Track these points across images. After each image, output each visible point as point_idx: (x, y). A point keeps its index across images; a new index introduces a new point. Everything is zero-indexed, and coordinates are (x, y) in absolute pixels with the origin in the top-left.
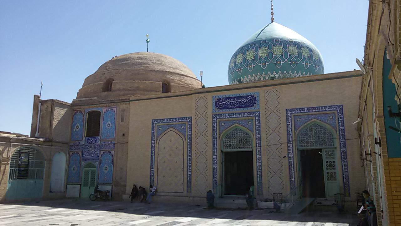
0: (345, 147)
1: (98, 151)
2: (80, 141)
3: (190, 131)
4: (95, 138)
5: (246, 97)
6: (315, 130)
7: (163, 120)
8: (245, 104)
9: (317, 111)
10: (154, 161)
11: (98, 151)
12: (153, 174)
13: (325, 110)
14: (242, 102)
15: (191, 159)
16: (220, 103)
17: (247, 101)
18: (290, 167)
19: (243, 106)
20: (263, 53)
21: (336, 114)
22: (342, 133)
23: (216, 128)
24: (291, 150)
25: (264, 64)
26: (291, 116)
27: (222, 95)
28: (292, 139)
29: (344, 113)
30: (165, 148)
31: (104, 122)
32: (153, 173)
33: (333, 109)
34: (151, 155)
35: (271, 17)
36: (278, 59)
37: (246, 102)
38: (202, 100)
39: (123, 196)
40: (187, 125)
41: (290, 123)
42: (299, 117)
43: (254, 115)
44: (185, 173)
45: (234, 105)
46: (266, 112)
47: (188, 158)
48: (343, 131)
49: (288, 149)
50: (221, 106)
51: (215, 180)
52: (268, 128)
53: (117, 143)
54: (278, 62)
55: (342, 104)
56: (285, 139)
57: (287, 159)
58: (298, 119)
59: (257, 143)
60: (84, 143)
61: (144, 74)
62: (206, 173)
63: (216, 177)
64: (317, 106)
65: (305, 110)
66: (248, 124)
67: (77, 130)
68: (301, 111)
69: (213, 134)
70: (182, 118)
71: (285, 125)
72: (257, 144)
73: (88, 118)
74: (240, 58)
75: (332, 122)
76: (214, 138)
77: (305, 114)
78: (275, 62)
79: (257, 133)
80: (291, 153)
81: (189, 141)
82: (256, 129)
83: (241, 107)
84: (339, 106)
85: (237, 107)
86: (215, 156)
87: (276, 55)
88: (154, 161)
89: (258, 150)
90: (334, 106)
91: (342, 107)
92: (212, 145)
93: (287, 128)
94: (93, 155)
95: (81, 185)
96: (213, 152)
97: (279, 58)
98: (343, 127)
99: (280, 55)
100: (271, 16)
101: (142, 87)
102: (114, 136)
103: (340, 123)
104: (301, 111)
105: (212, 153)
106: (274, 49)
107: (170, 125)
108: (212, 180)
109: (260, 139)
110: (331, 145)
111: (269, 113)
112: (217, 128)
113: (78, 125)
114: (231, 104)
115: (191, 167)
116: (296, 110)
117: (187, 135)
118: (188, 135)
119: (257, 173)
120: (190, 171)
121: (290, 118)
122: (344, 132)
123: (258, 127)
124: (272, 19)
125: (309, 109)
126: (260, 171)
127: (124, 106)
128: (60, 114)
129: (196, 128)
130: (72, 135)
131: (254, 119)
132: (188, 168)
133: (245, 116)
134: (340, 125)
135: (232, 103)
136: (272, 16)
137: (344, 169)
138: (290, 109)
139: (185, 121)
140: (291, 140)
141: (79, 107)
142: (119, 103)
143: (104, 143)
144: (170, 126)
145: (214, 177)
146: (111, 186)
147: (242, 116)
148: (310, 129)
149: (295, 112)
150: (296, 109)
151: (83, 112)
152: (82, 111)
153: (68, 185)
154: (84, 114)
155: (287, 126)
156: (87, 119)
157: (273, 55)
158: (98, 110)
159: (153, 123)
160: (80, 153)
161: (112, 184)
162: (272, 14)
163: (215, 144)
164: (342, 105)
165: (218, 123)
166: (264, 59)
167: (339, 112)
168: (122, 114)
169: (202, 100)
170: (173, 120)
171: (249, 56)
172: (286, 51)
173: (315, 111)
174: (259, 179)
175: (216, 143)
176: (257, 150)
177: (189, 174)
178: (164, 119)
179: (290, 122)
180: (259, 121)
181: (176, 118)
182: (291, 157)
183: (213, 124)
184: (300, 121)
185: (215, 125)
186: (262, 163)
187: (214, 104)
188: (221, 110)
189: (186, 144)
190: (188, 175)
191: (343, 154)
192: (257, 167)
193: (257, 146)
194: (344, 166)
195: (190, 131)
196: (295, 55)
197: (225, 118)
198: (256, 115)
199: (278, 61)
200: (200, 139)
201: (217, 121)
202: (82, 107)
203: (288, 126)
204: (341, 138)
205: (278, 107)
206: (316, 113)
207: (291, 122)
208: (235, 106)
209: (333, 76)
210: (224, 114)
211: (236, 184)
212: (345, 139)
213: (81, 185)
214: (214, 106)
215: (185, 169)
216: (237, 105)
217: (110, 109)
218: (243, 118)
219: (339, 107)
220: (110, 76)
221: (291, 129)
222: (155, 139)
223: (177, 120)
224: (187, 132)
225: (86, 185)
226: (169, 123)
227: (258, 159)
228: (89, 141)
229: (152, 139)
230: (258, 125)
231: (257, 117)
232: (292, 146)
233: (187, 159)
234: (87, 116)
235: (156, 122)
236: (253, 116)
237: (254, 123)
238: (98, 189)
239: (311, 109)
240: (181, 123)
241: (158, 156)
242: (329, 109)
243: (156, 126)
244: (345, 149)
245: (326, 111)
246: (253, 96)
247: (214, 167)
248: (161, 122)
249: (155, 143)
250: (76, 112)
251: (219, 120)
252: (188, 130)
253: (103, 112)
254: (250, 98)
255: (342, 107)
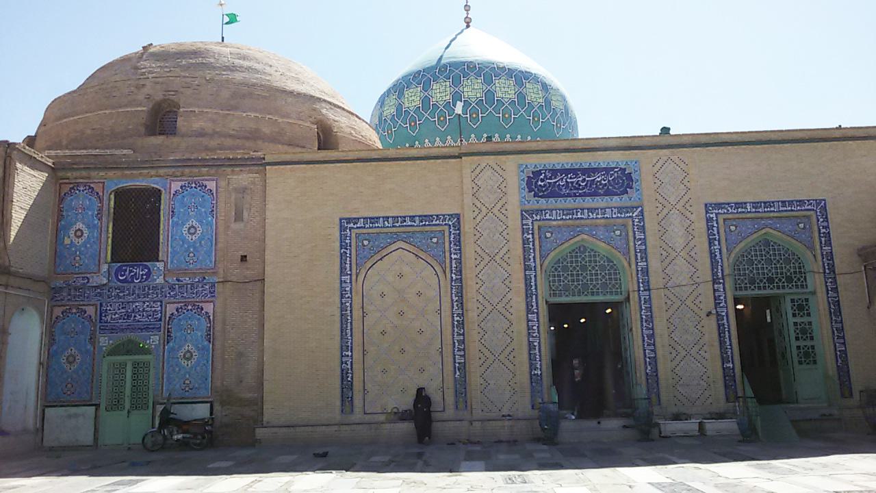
0: (835, 290)
1: (159, 303)
2: (88, 276)
3: (455, 250)
4: (146, 267)
5: (607, 170)
6: (583, 259)
7: (374, 220)
8: (606, 188)
9: (774, 211)
10: (351, 329)
11: (159, 303)
12: (349, 367)
13: (790, 208)
14: (598, 182)
15: (463, 324)
16: (540, 183)
17: (609, 181)
18: (720, 337)
19: (600, 191)
20: (440, 92)
21: (814, 219)
22: (828, 259)
23: (531, 244)
24: (722, 298)
25: (474, 116)
26: (717, 220)
27: (544, 162)
28: (722, 274)
29: (829, 217)
30: (383, 295)
31: (175, 219)
32: (349, 363)
33: (806, 207)
34: (342, 315)
35: (466, 16)
36: (441, 109)
37: (606, 182)
38: (488, 173)
39: (258, 431)
40: (447, 234)
41: (715, 235)
42: (734, 223)
43: (628, 215)
44: (448, 359)
45: (578, 189)
46: (659, 210)
47: (453, 320)
48: (831, 255)
49: (715, 297)
50: (544, 189)
51: (535, 374)
52: (664, 246)
53: (222, 282)
54: (505, 114)
55: (823, 198)
56: (705, 273)
57: (713, 318)
58: (731, 227)
59: (641, 281)
60: (105, 281)
61: (265, 97)
62: (511, 357)
63: (539, 366)
64: (773, 200)
65: (749, 207)
66: (370, 246)
67: (76, 240)
68: (740, 210)
69: (525, 258)
70: (432, 216)
71: (705, 239)
72: (641, 285)
73: (114, 209)
74: (413, 98)
75: (804, 236)
76: (527, 268)
77: (749, 215)
78: (482, 117)
79: (639, 258)
80: (721, 305)
81: (453, 275)
82: (635, 249)
83: (594, 194)
84: (818, 202)
85: (585, 195)
86: (533, 313)
87: (502, 98)
88: (351, 329)
89: (642, 299)
90: (808, 201)
91: (825, 204)
92: (523, 286)
93: (710, 247)
94: (138, 317)
95: (97, 406)
96: (527, 305)
97: (473, 104)
98: (830, 248)
99: (510, 99)
100: (466, 12)
101: (266, 130)
102: (211, 262)
103: (823, 239)
104: (740, 210)
105: (523, 306)
106: (497, 85)
107: (396, 233)
108: (528, 376)
109: (646, 271)
110: (802, 286)
111: (665, 211)
112: (533, 245)
113: (80, 225)
114: (570, 185)
115: (464, 343)
116: (727, 206)
117: (448, 261)
118: (451, 262)
119: (645, 353)
120: (462, 353)
121: (715, 225)
122: (832, 259)
123: (640, 242)
124: (467, 20)
125: (756, 205)
126: (652, 347)
127: (243, 178)
128: (29, 188)
129: (478, 242)
130: (57, 255)
131: (631, 223)
132: (454, 347)
133: (606, 216)
134: (823, 242)
135: (572, 183)
136: (468, 14)
137: (836, 338)
138: (715, 204)
139: (441, 225)
140: (720, 275)
141: (84, 173)
142: (229, 170)
143: (178, 280)
144: (396, 238)
145: (532, 367)
146: (209, 405)
147: (600, 216)
148: (756, 251)
149: (725, 211)
150: (728, 204)
151: (98, 188)
152: (92, 185)
153: (47, 410)
154: (101, 194)
155: (710, 243)
156: (112, 210)
157: (496, 99)
158: (155, 186)
159: (342, 229)
160: (91, 311)
161: (210, 400)
162: (467, 8)
163: (533, 284)
164: (824, 200)
165: (536, 232)
166: (476, 104)
167: (818, 214)
168: (236, 199)
169: (488, 173)
170: (405, 221)
171: (438, 95)
172: (521, 92)
173: (769, 209)
174: (649, 368)
175: (533, 281)
176: (640, 298)
177: (459, 363)
178: (378, 218)
179: (715, 232)
180: (643, 229)
181: (414, 217)
182: (724, 314)
183: (523, 234)
184: (552, 238)
185: (530, 236)
186: (655, 331)
187: (525, 184)
188: (543, 200)
189: (446, 284)
190: (457, 365)
191: (832, 306)
192: (644, 341)
193: (642, 289)
194: (836, 332)
195: (455, 250)
196: (539, 103)
197: (554, 220)
198: (634, 215)
199: (440, 115)
200: (489, 271)
201: (533, 226)
202: (94, 174)
203: (711, 243)
204: (827, 271)
205: (686, 198)
206: (772, 214)
207: (718, 233)
208: (580, 192)
209: (800, 135)
210: (551, 210)
211: (591, 382)
212: (834, 272)
213: (97, 406)
214: (524, 189)
215: (448, 350)
216: (584, 188)
217: (194, 185)
218: (602, 221)
219: (818, 204)
220: (164, 93)
221: (720, 250)
222: (351, 270)
223: (417, 222)
224: (447, 254)
225: (116, 405)
226: (394, 230)
227: (644, 320)
228: (122, 276)
229: (341, 272)
230: (640, 239)
231: (637, 220)
232: (724, 289)
233: (451, 324)
234: (112, 203)
235: (352, 225)
236: (627, 217)
237: (631, 234)
238: (172, 416)
239: (761, 206)
240: (428, 228)
241: (363, 316)
242: (798, 208)
243: (353, 235)
244: (835, 295)
245: (792, 210)
246: (625, 169)
247: (533, 342)
248: (367, 226)
249: (351, 282)
250: (73, 188)
251: (541, 223)
252: (450, 248)
253: (173, 192)
254: (616, 174)
255: (825, 204)
